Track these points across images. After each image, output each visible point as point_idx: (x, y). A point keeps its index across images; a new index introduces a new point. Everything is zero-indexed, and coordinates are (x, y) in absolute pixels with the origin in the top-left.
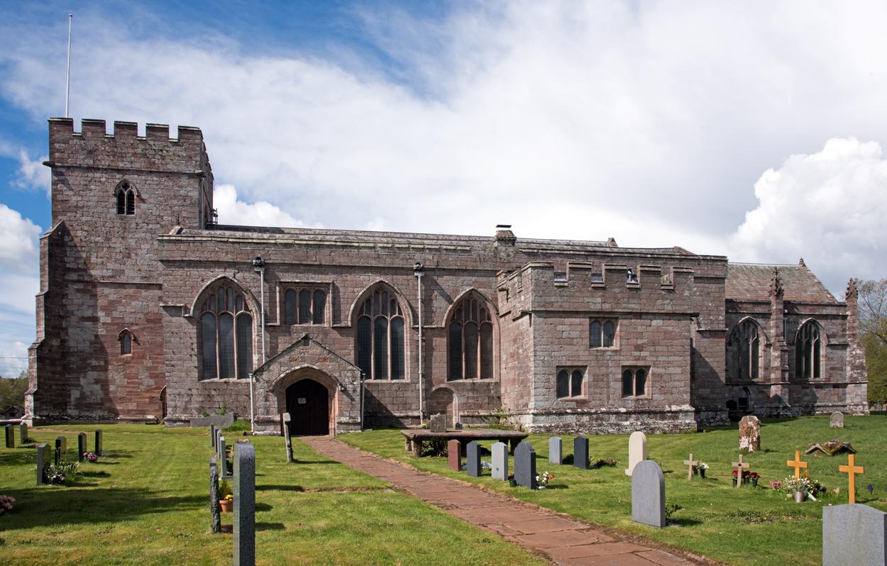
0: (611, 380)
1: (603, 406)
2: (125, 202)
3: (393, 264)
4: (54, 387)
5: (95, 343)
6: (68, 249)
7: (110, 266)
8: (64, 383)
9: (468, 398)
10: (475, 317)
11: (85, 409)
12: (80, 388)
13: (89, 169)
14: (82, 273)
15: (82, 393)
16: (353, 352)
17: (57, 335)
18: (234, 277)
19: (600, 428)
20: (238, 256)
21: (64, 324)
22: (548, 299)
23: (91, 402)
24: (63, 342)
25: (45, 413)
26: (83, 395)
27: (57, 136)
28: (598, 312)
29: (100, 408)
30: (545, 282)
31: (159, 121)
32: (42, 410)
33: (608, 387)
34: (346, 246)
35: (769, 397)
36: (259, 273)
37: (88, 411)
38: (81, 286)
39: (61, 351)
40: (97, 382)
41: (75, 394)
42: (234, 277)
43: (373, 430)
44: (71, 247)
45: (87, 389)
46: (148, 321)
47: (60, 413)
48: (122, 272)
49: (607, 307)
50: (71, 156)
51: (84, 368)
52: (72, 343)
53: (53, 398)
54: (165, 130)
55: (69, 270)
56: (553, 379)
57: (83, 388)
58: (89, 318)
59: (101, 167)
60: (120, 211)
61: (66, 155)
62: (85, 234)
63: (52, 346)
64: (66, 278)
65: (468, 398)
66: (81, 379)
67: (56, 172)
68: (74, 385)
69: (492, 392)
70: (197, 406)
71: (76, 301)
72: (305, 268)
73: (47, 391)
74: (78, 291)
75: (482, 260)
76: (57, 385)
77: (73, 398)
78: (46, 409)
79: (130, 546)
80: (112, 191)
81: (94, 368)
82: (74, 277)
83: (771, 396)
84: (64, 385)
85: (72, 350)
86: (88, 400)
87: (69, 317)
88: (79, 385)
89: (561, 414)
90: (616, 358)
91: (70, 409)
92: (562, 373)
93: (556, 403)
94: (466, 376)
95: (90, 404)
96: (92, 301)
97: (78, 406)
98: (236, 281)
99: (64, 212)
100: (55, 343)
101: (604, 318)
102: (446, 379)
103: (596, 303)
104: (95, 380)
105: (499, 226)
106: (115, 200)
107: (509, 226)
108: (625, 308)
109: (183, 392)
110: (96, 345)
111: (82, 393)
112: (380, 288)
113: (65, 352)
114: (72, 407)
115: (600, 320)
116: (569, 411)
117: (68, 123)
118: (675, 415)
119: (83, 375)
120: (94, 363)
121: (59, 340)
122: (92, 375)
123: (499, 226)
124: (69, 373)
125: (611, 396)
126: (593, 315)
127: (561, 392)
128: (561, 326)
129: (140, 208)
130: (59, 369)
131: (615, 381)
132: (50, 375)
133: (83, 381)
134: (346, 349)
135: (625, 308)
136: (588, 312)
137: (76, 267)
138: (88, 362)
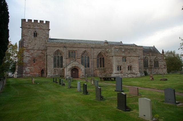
2: (35, 35)
6: (24, 43)
7: (32, 47)
10: (101, 56)
13: (29, 28)
27: (23, 22)
34: (80, 44)
40: (29, 69)
41: (24, 71)
45: (27, 70)
46: (39, 57)
48: (34, 48)
49: (125, 55)
54: (37, 21)
56: (117, 68)
60: (34, 36)
64: (161, 53)
74: (26, 51)
79: (59, 91)
81: (28, 66)
86: (27, 73)
89: (118, 74)
92: (118, 67)
93: (118, 72)
97: (25, 74)
99: (24, 36)
103: (123, 55)
112: (85, 52)
117: (25, 20)
118: (137, 74)
127: (118, 70)
129: (38, 36)
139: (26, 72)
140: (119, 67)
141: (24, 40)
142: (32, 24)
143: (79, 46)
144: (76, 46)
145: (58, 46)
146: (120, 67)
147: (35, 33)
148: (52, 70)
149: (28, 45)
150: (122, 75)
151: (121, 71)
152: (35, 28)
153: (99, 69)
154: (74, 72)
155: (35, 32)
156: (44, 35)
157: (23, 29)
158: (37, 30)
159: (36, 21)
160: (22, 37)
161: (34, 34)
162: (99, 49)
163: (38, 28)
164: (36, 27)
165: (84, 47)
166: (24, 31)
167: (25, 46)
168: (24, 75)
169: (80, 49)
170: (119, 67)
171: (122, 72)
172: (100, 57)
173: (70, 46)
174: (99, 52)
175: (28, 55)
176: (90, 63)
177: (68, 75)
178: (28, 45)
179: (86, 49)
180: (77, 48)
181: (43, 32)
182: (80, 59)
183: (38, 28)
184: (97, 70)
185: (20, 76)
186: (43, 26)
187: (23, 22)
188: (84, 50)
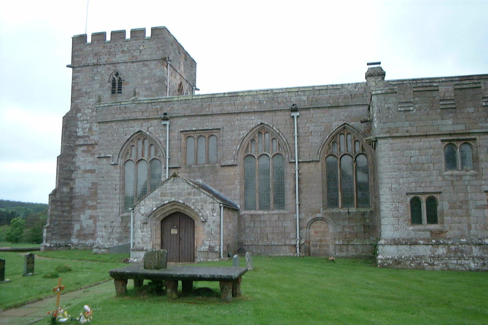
0: (471, 207)
1: (462, 236)
3: (272, 107)
4: (62, 222)
5: (91, 189)
6: (79, 123)
8: (70, 219)
9: (344, 227)
11: (83, 238)
12: (80, 223)
14: (87, 139)
15: (81, 226)
16: (238, 187)
17: (66, 184)
18: (148, 131)
19: (459, 262)
20: (151, 114)
21: (73, 176)
22: (392, 125)
23: (87, 233)
24: (71, 189)
25: (55, 242)
26: (82, 229)
28: (450, 135)
29: (92, 237)
30: (388, 108)
31: (138, 26)
32: (52, 239)
33: (468, 215)
35: (152, 283)
36: (165, 125)
37: (84, 239)
38: (85, 148)
39: (69, 195)
40: (91, 217)
41: (77, 227)
42: (148, 131)
43: (125, 272)
44: (80, 120)
45: (84, 224)
47: (65, 241)
49: (460, 128)
50: (84, 59)
51: (84, 207)
52: (77, 190)
53: (61, 230)
54: (143, 31)
55: (79, 137)
57: (82, 223)
58: (89, 170)
59: (102, 63)
60: (113, 92)
61: (81, 59)
62: (90, 111)
63: (63, 192)
65: (344, 227)
66: (81, 215)
67: (75, 71)
68: (76, 221)
69: (368, 220)
70: (117, 236)
71: (81, 159)
72: (201, 118)
73: (57, 225)
74: (84, 151)
75: (353, 96)
76: (64, 220)
77: (75, 229)
78: (56, 239)
80: (107, 79)
81: (90, 207)
82: (81, 142)
83: (144, 285)
84: (69, 221)
85: (77, 195)
86: (85, 232)
87: (77, 170)
88: (79, 221)
89: (414, 243)
90: (476, 182)
91: (73, 238)
92: (415, 203)
94: (260, 207)
95: (86, 234)
96: (92, 158)
97: (78, 236)
98: (148, 133)
99: (78, 97)
100: (65, 190)
101: (458, 140)
102: (322, 209)
104: (90, 216)
105: (368, 64)
106: (110, 85)
107: (379, 63)
108: (482, 128)
109: (108, 224)
110: (92, 190)
111: (81, 226)
113: (71, 196)
114: (74, 237)
115: (454, 143)
116: (422, 242)
119: (82, 213)
120: (90, 203)
121: (69, 188)
122: (88, 212)
123: (368, 64)
124: (74, 212)
125: (473, 226)
126: (445, 138)
127: (416, 219)
128: (408, 152)
130: (67, 208)
131: (477, 208)
132: (60, 213)
133: (82, 217)
134: (233, 184)
135: (482, 128)
136: (439, 135)
137: (83, 135)
138: (87, 203)
139: (82, 229)
140: (424, 206)
141: (78, 111)
142: (104, 47)
143: (230, 109)
144: (216, 110)
145: (139, 115)
146: (432, 202)
147: (117, 79)
148: (115, 224)
149: (90, 129)
150: (441, 251)
151: (433, 227)
152: (114, 60)
153: (336, 217)
154: (174, 231)
155: (117, 74)
156: (147, 82)
157: (79, 71)
158: (121, 68)
159: (118, 35)
160: (73, 99)
161: (114, 84)
162: (334, 110)
163: (126, 58)
164: (119, 57)
165: (256, 108)
166: (81, 76)
167: (80, 133)
168: (74, 241)
169: (237, 120)
170: (424, 206)
171: (441, 232)
172: (149, 155)
173: (188, 113)
174: (336, 125)
175: (89, 166)
176: (288, 185)
177: (141, 246)
178: (90, 129)
179: (267, 119)
180: (221, 118)
181: (142, 72)
182: (237, 170)
183: (126, 57)
184: (322, 219)
185: (58, 246)
186: (141, 48)
187: (77, 47)
188: (255, 120)
